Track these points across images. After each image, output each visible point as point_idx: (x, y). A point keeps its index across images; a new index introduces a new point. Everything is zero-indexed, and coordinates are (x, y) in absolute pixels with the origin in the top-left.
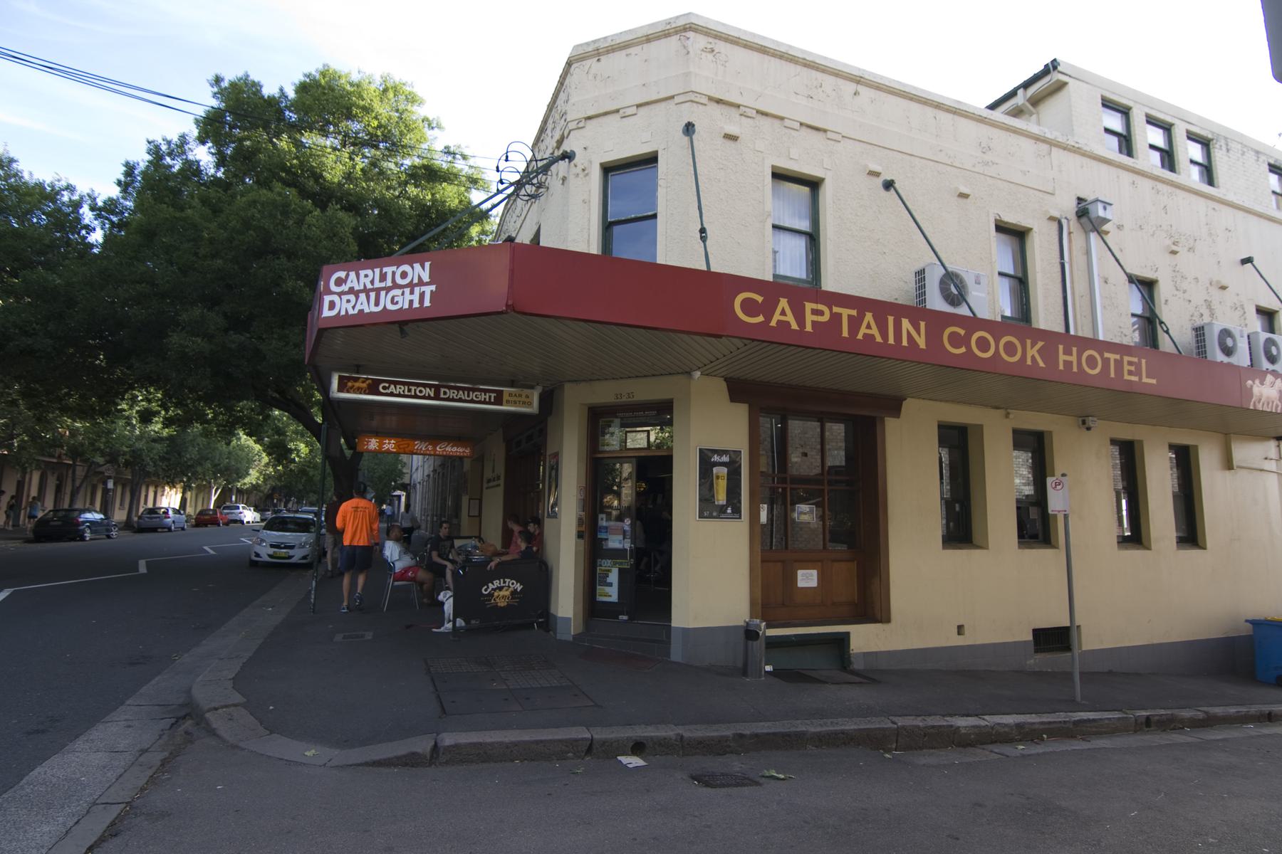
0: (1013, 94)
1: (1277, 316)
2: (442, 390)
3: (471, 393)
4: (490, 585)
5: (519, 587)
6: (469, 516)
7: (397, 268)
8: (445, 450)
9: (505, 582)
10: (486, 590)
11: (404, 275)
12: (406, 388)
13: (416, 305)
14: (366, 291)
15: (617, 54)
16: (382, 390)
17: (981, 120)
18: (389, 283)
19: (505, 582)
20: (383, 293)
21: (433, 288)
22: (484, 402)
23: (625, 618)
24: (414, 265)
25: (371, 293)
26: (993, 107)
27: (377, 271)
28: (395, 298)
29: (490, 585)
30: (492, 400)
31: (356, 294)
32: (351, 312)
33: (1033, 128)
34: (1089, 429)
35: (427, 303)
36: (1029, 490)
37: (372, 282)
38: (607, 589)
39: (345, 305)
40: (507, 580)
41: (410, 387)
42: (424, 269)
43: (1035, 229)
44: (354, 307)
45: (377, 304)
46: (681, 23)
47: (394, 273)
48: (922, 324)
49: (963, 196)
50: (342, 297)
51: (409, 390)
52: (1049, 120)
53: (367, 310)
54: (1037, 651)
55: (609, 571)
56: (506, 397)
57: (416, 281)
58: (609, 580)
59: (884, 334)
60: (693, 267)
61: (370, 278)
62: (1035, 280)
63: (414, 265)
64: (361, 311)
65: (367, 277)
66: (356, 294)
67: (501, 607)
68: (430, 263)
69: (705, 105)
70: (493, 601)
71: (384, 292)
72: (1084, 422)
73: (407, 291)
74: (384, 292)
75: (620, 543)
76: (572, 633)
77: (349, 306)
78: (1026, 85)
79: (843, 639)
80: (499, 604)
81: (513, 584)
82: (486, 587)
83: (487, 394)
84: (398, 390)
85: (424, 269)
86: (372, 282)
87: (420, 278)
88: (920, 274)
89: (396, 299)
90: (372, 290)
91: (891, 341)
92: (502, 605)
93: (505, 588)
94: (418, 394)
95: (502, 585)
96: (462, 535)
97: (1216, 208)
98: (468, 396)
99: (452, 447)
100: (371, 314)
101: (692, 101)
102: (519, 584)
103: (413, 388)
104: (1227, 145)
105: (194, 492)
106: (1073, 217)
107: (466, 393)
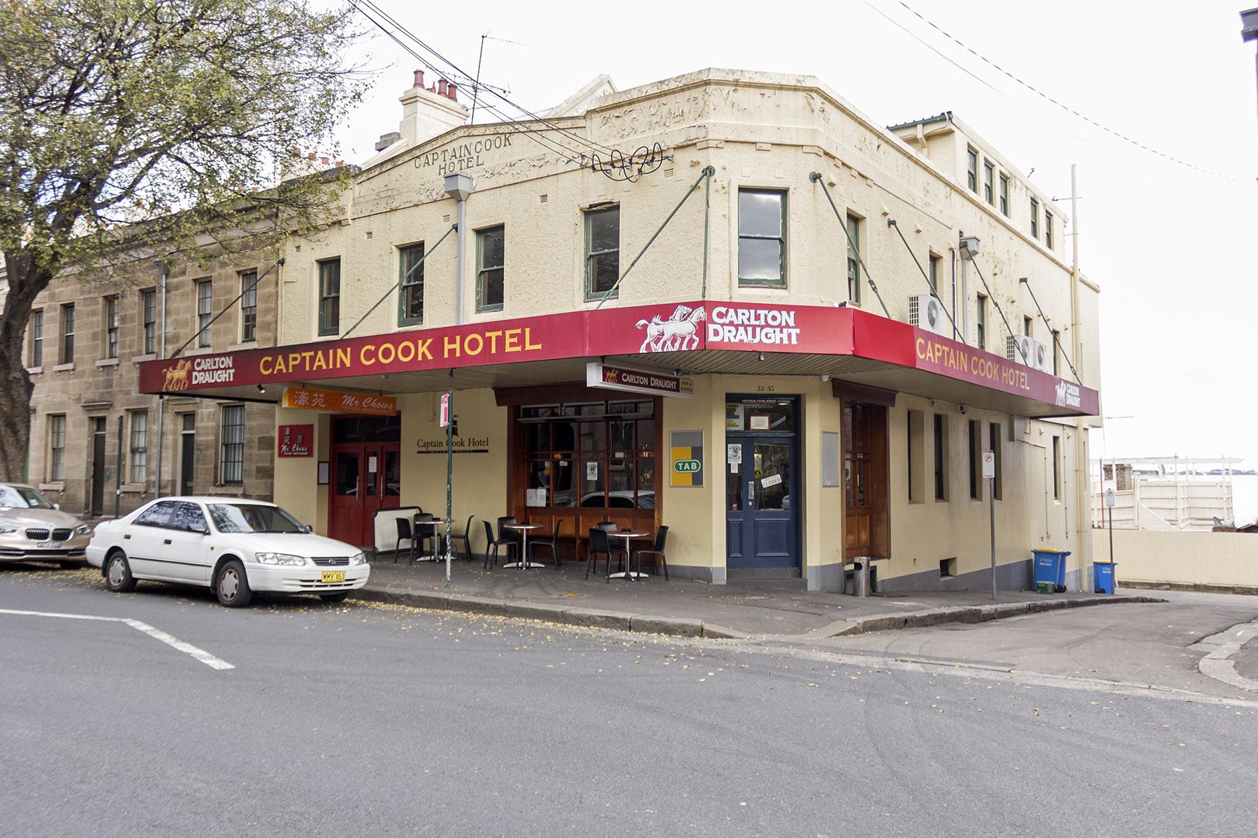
0: (914, 125)
1: (1030, 322)
6: (318, 484)
8: (370, 407)
13: (786, 341)
15: (752, 90)
17: (879, 136)
18: (763, 323)
20: (758, 329)
26: (894, 129)
31: (737, 327)
32: (733, 340)
33: (922, 157)
34: (963, 413)
35: (794, 341)
37: (749, 319)
39: (727, 334)
41: (759, 312)
49: (918, 231)
51: (757, 317)
52: (936, 157)
57: (784, 324)
60: (875, 314)
61: (747, 316)
64: (742, 341)
66: (737, 327)
72: (962, 408)
73: (778, 330)
78: (925, 123)
86: (749, 319)
96: (401, 506)
99: (377, 402)
100: (749, 344)
103: (762, 313)
106: (958, 248)
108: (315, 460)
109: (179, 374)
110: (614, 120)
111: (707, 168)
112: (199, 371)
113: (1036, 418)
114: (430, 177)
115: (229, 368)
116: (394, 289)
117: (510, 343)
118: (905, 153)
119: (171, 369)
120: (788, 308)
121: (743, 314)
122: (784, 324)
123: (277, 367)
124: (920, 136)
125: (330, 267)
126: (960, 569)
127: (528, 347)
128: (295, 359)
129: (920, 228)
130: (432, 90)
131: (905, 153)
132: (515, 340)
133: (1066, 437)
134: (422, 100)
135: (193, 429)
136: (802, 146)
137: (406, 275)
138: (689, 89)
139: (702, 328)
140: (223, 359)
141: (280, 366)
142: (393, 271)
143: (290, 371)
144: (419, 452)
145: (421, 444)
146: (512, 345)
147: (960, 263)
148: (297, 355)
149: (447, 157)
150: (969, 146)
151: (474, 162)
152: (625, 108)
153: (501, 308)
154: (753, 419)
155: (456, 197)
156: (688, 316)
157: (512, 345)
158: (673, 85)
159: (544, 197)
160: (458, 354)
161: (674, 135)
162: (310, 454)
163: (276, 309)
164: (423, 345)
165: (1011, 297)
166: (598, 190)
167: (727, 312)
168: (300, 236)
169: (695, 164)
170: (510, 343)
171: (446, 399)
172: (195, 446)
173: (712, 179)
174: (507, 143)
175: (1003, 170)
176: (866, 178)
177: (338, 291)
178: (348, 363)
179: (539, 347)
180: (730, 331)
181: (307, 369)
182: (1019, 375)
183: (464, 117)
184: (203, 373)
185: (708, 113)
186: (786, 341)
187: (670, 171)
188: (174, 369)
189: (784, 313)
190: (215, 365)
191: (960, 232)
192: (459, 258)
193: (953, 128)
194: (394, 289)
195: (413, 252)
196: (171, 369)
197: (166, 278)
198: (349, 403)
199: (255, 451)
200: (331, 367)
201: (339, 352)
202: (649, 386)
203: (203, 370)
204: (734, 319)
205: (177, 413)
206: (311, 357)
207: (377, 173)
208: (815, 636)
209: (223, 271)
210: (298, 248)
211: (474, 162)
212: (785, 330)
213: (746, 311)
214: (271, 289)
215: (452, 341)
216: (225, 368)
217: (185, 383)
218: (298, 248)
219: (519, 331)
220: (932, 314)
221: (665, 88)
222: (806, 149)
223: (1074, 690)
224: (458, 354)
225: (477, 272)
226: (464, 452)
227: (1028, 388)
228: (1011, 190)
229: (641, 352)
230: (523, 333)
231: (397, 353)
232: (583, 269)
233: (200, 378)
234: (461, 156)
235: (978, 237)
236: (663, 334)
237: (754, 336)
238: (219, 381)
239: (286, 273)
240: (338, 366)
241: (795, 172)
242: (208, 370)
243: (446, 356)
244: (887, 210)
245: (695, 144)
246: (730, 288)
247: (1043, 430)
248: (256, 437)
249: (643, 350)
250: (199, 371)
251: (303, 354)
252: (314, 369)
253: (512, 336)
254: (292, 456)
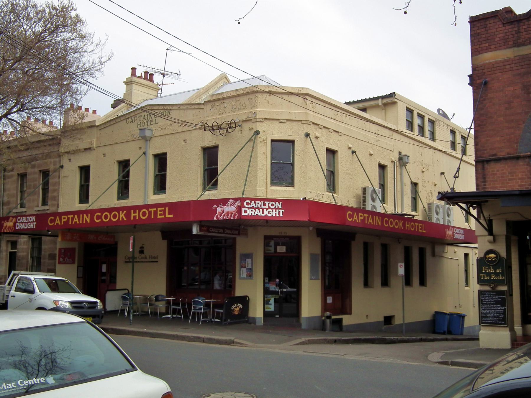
0: (378, 98)
12: (262, 202)
13: (277, 215)
16: (211, 231)
18: (267, 207)
20: (265, 210)
23: (278, 316)
31: (255, 209)
32: (253, 215)
34: (400, 243)
35: (281, 215)
37: (261, 206)
38: (269, 306)
39: (251, 212)
40: (238, 304)
41: (265, 202)
43: (388, 166)
44: (254, 213)
46: (304, 92)
48: (380, 217)
49: (371, 155)
51: (265, 205)
53: (259, 215)
54: (385, 324)
55: (271, 299)
57: (277, 207)
58: (270, 303)
59: (373, 223)
62: (387, 186)
69: (311, 125)
72: (398, 241)
75: (275, 288)
77: (253, 213)
78: (383, 97)
79: (340, 320)
86: (261, 206)
88: (364, 189)
89: (270, 212)
91: (374, 224)
96: (117, 288)
97: (512, 366)
101: (308, 124)
103: (267, 203)
104: (439, 123)
105: (35, 267)
106: (397, 160)
108: (75, 266)
109: (10, 224)
110: (216, 107)
111: (256, 132)
112: (19, 223)
113: (452, 244)
114: (133, 129)
115: (34, 222)
116: (133, 164)
117: (160, 214)
118: (362, 118)
119: (6, 221)
120: (279, 201)
121: (258, 203)
122: (277, 207)
123: (56, 222)
124: (380, 104)
125: (85, 171)
126: (398, 321)
127: (167, 216)
128: (64, 218)
129: (372, 152)
130: (140, 77)
131: (362, 118)
132: (162, 213)
133: (474, 254)
134: (135, 83)
135: (16, 249)
136: (301, 120)
137: (122, 175)
138: (249, 94)
139: (239, 209)
140: (31, 217)
141: (58, 221)
142: (114, 174)
143: (62, 224)
144: (126, 262)
145: (127, 258)
146: (161, 215)
147: (399, 170)
148: (65, 217)
149: (141, 119)
150: (407, 108)
151: (154, 122)
152: (221, 101)
153: (165, 193)
154: (278, 248)
155: (146, 139)
156: (234, 204)
157: (161, 215)
158: (242, 92)
159: (185, 141)
160: (137, 218)
161: (242, 115)
162: (73, 262)
163: (58, 190)
164: (122, 213)
165: (434, 183)
166: (209, 140)
167: (251, 202)
168: (71, 154)
169: (251, 129)
170: (160, 214)
171: (132, 239)
172: (17, 258)
173: (259, 136)
174: (169, 114)
175: (430, 118)
176: (338, 132)
177: (89, 181)
178: (89, 221)
179: (172, 216)
180: (252, 211)
181: (70, 223)
182: (418, 226)
183: (157, 90)
184: (21, 224)
185: (257, 106)
186: (277, 215)
187: (240, 131)
188: (7, 221)
189: (277, 203)
190: (27, 220)
191: (399, 152)
192: (146, 168)
193: (396, 100)
194: (133, 164)
195: (125, 165)
196: (6, 221)
197: (4, 173)
198: (91, 238)
199: (47, 261)
200: (81, 222)
201: (85, 216)
202: (224, 233)
203: (21, 223)
205: (8, 241)
206: (72, 217)
207: (108, 125)
208: (287, 345)
209: (33, 170)
210: (70, 160)
211: (154, 122)
212: (277, 210)
213: (259, 202)
214: (56, 180)
215: (135, 212)
216: (32, 222)
217: (12, 229)
218: (70, 160)
219: (163, 209)
220: (373, 196)
221: (238, 93)
222: (303, 122)
224: (137, 218)
225: (154, 175)
226: (147, 262)
227: (425, 231)
228: (437, 127)
229: (214, 219)
230: (165, 209)
231: (110, 217)
232: (202, 175)
233: (20, 226)
234: (147, 119)
235: (408, 155)
237: (263, 213)
238: (29, 228)
239: (64, 172)
240: (84, 222)
241: (298, 133)
242: (24, 223)
243: (132, 219)
244: (350, 146)
245: (251, 120)
246: (266, 186)
247: (456, 250)
248: (47, 254)
249: (215, 219)
250: (19, 223)
251: (69, 216)
252: (73, 223)
253: (160, 211)
254: (65, 263)
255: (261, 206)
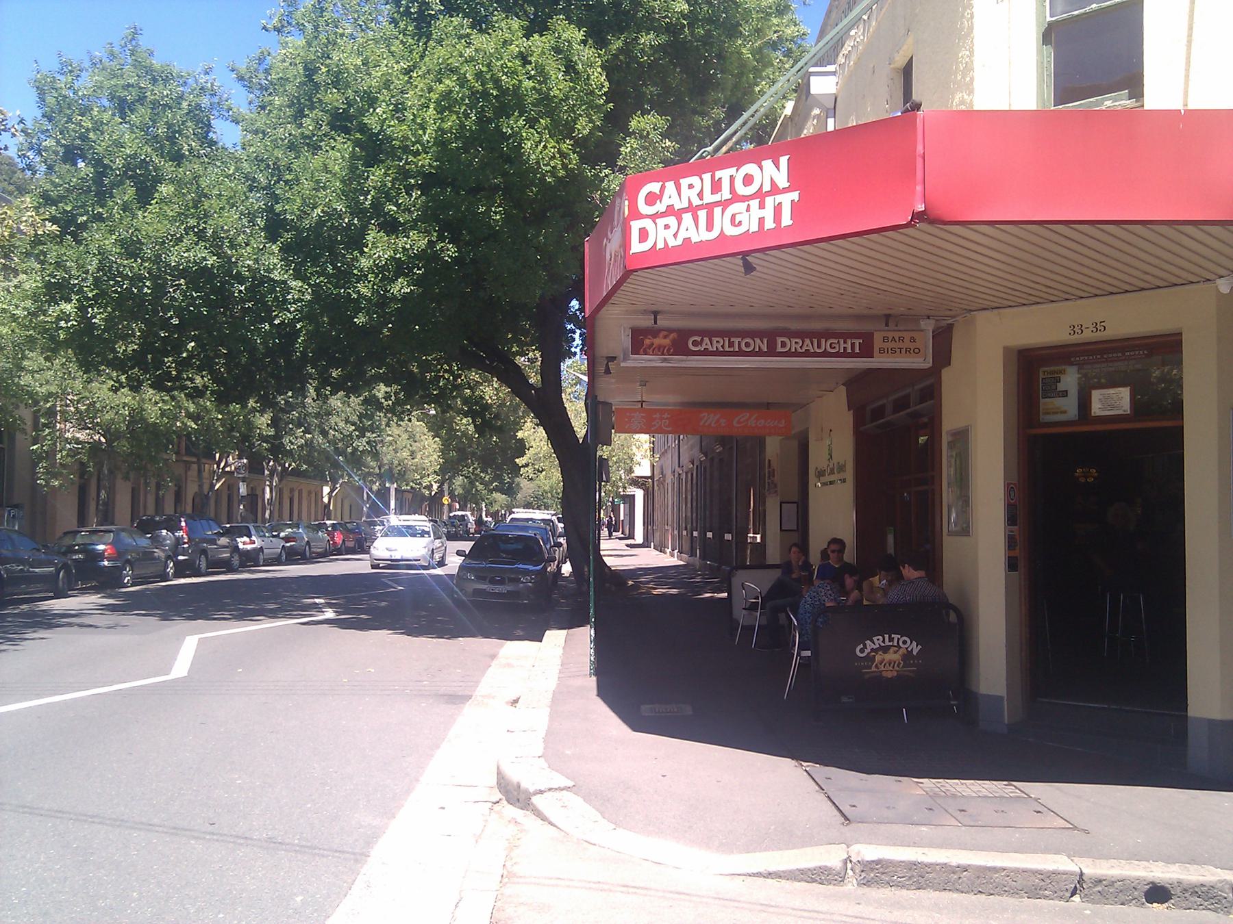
2: (779, 340)
3: (823, 341)
4: (868, 642)
5: (915, 648)
7: (737, 170)
9: (891, 640)
10: (862, 651)
11: (748, 180)
12: (727, 340)
13: (770, 224)
14: (692, 209)
19: (891, 640)
21: (795, 195)
22: (844, 354)
24: (764, 163)
25: (699, 213)
27: (707, 177)
28: (737, 216)
29: (868, 642)
30: (857, 350)
31: (678, 214)
32: (672, 243)
35: (786, 220)
36: (531, 791)
37: (700, 195)
39: (663, 233)
41: (732, 340)
42: (778, 167)
44: (675, 235)
45: (710, 227)
47: (732, 179)
50: (657, 220)
51: (731, 344)
53: (695, 239)
56: (878, 342)
57: (767, 188)
61: (697, 189)
63: (764, 163)
64: (687, 241)
65: (693, 188)
66: (678, 214)
67: (887, 679)
68: (787, 157)
70: (873, 669)
71: (720, 208)
73: (754, 203)
74: (720, 208)
76: (1006, 722)
77: (669, 234)
80: (884, 674)
81: (905, 642)
82: (861, 646)
83: (849, 342)
84: (714, 344)
85: (778, 167)
86: (700, 195)
87: (772, 181)
90: (700, 207)
92: (889, 675)
93: (892, 649)
94: (744, 348)
95: (887, 643)
98: (819, 347)
102: (914, 643)
103: (736, 341)
107: (815, 341)
167: (702, 340)
204: (709, 347)
223: (844, 553)
236: (884, 660)
255: (701, 199)
